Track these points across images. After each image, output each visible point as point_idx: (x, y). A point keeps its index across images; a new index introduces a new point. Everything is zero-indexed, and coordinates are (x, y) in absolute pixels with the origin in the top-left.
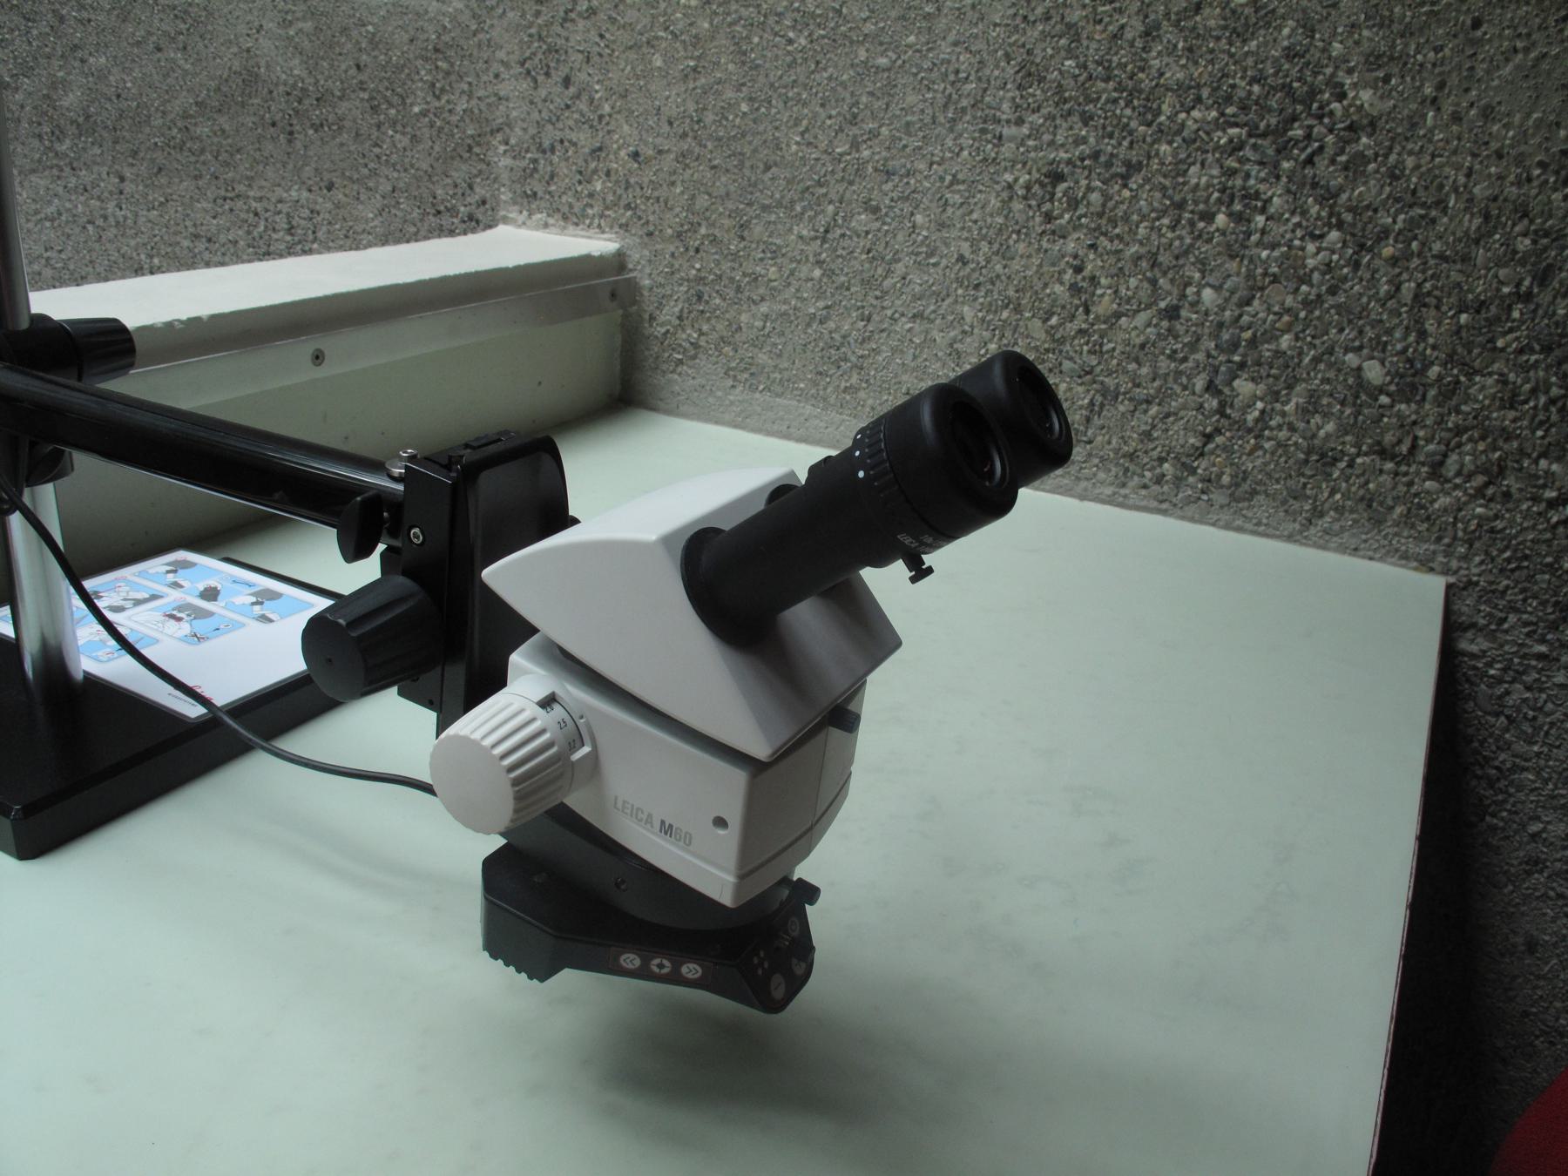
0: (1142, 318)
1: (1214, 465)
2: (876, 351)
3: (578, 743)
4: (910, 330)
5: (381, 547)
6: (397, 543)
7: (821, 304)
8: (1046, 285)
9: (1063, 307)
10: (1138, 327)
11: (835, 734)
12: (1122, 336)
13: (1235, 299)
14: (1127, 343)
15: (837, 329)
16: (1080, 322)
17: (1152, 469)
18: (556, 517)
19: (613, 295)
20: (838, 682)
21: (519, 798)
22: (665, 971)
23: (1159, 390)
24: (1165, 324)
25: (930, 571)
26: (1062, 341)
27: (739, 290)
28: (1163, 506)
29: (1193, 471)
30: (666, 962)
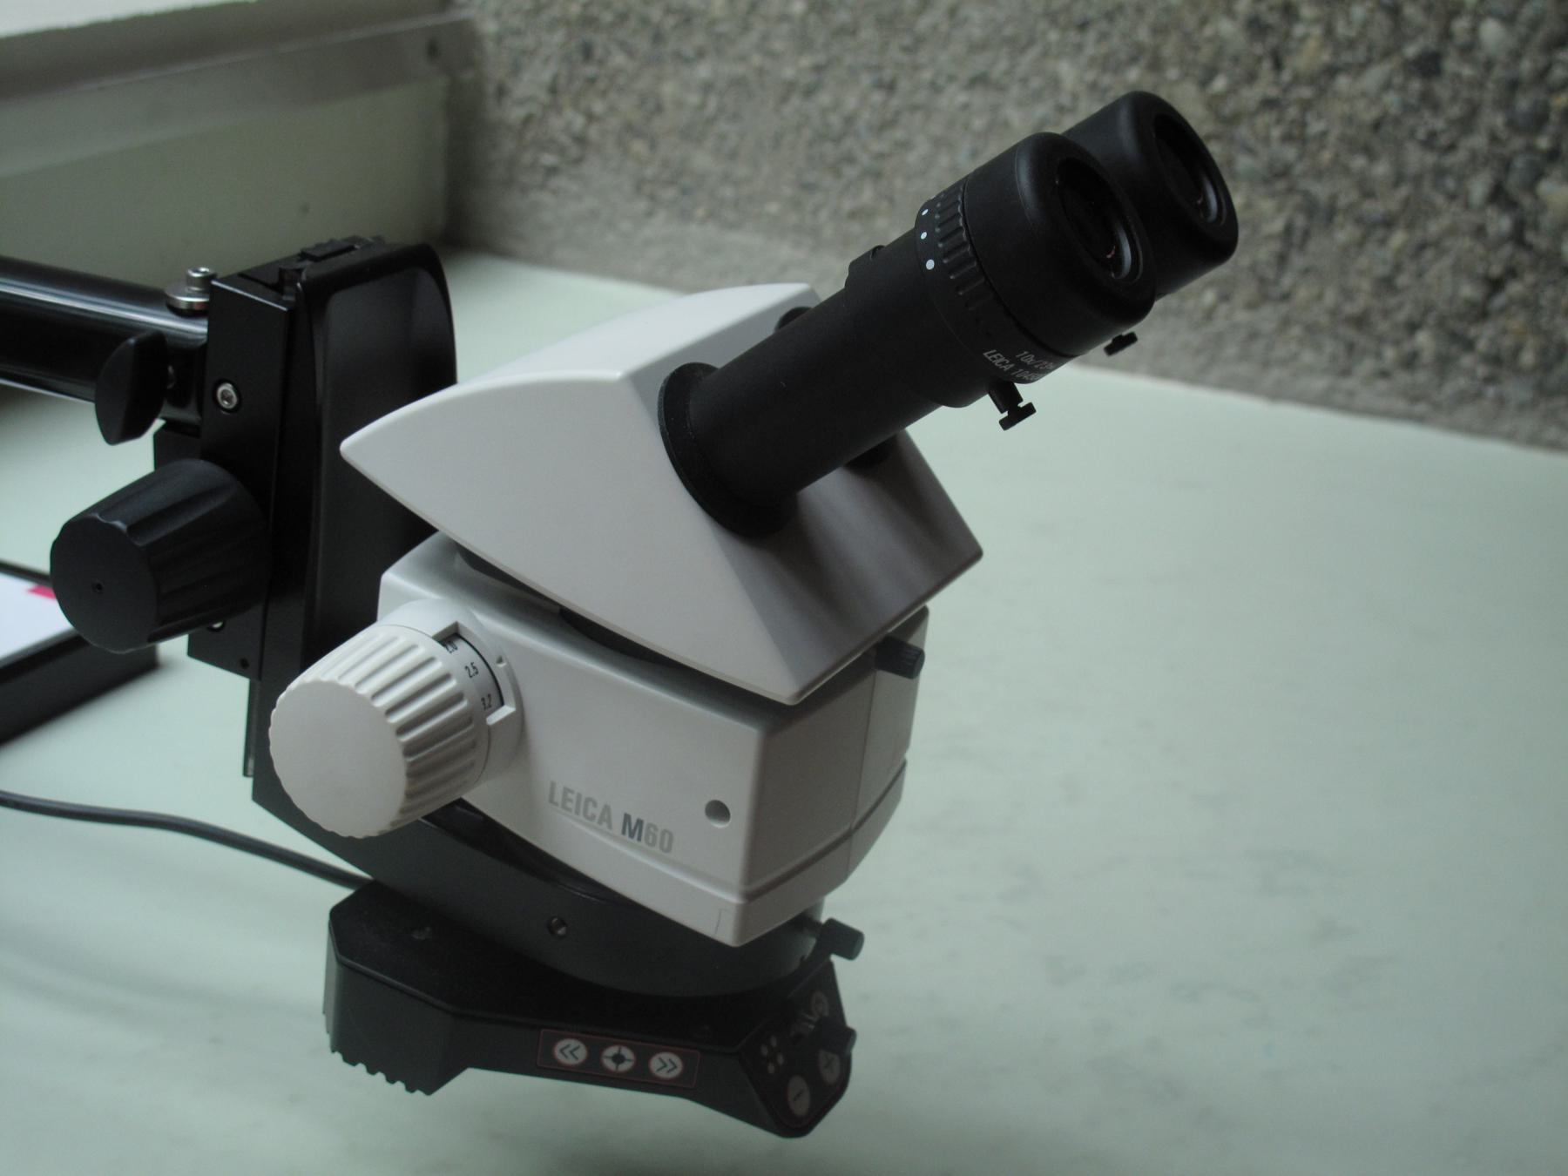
0: (1374, 77)
1: (1505, 332)
2: (905, 145)
3: (495, 700)
4: (966, 107)
5: (158, 424)
6: (189, 415)
7: (806, 61)
8: (1204, 21)
9: (1236, 59)
10: (1368, 90)
11: (887, 681)
12: (1339, 108)
13: (1540, 36)
14: (1349, 120)
15: (836, 106)
16: (1264, 87)
17: (1397, 343)
18: (436, 369)
19: (433, 50)
20: (891, 602)
21: (414, 774)
22: (625, 1067)
23: (1406, 202)
24: (1416, 85)
25: (1030, 410)
26: (1234, 119)
27: (658, 38)
28: (1419, 407)
29: (1469, 345)
30: (627, 1053)
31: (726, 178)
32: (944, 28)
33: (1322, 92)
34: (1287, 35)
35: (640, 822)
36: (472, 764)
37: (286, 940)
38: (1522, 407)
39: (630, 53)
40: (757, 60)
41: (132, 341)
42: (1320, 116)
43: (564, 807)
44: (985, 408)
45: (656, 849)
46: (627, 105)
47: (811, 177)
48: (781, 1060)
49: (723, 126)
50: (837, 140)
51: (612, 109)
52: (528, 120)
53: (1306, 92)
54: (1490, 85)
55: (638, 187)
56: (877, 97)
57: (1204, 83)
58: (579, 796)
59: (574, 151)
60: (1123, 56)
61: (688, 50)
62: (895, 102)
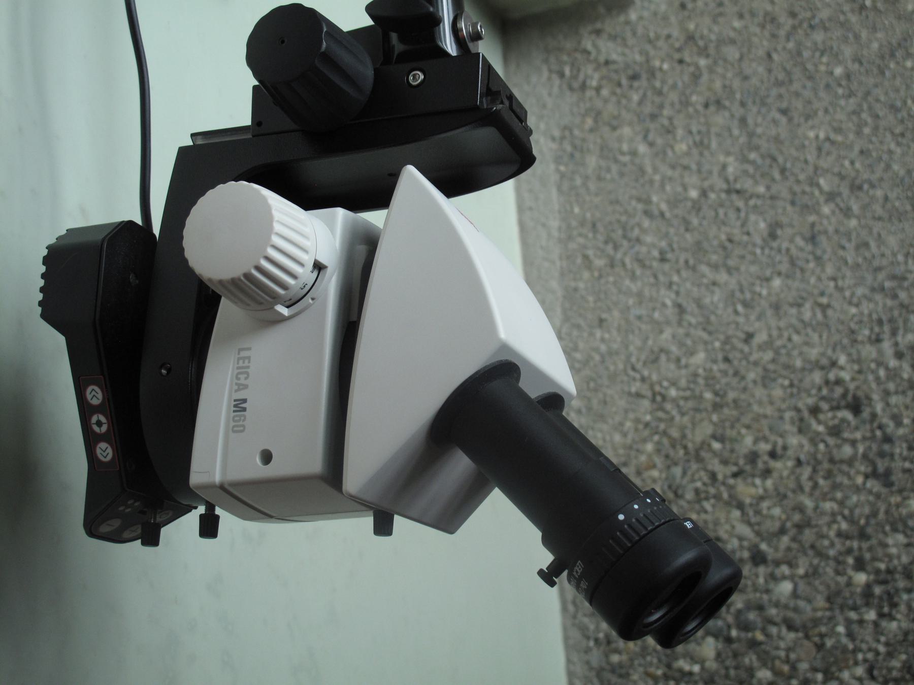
0: (744, 530)
2: (633, 277)
3: (288, 303)
4: (664, 305)
7: (664, 207)
8: (748, 427)
9: (732, 451)
13: (790, 614)
15: (643, 231)
16: (722, 471)
21: (234, 282)
22: (96, 428)
24: (746, 554)
26: (699, 459)
27: (653, 117)
30: (104, 428)
31: (586, 178)
32: (705, 281)
33: (728, 504)
34: (753, 476)
35: (244, 409)
36: (248, 305)
37: (102, 193)
38: (588, 663)
39: (640, 103)
40: (657, 178)
41: (431, 9)
42: (713, 506)
43: (239, 359)
44: (546, 558)
45: (232, 424)
46: (611, 108)
47: (600, 227)
48: (128, 510)
49: (614, 168)
50: (625, 236)
51: (606, 101)
52: (586, 52)
53: (725, 496)
54: (758, 595)
55: (565, 128)
56: (656, 253)
57: (714, 437)
58: (248, 367)
59: (576, 85)
60: (718, 387)
61: (651, 137)
62: (655, 264)
